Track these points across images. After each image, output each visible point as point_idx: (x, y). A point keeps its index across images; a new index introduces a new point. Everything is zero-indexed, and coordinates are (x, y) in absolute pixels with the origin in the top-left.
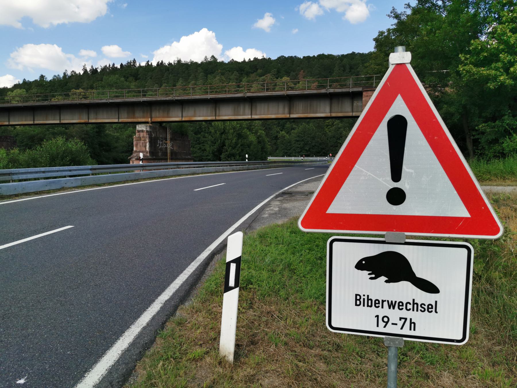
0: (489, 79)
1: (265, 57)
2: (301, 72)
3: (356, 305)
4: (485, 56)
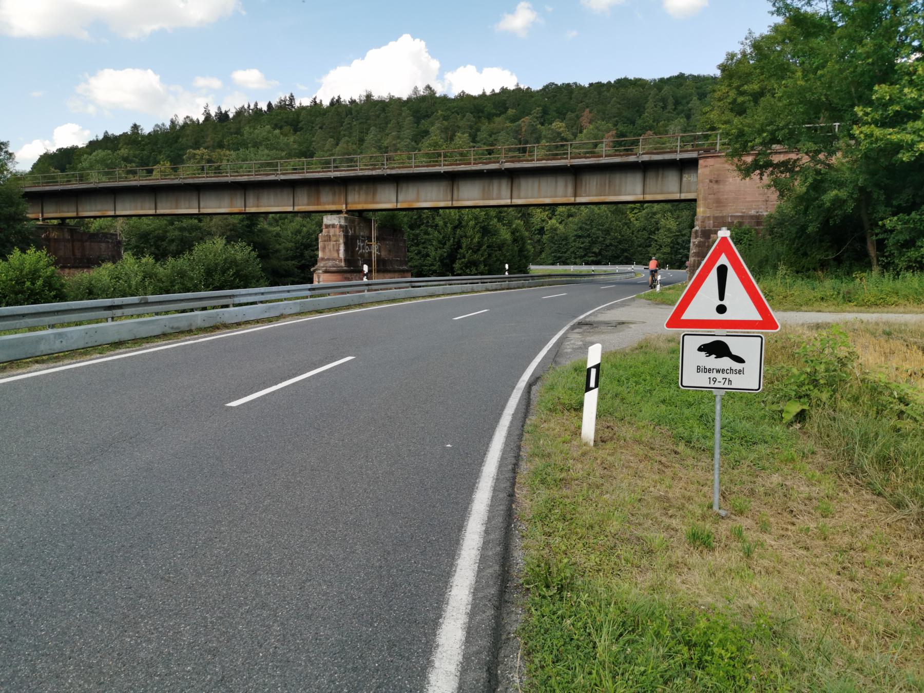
0: (901, 147)
4: (897, 111)
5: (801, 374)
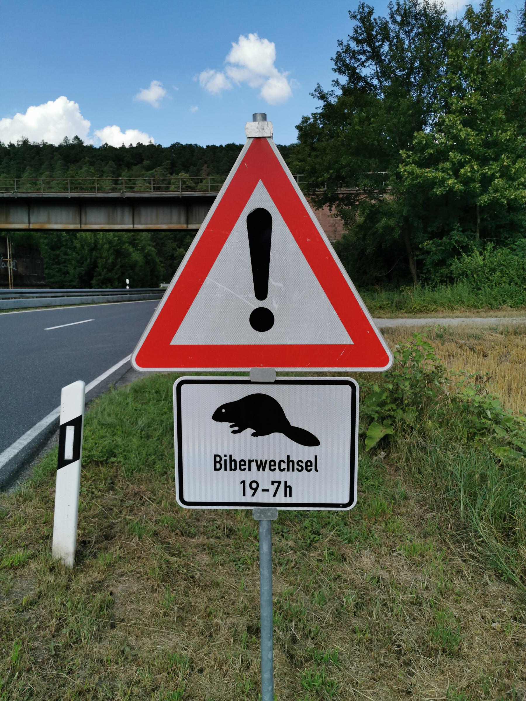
0: (435, 183)
1: (153, 142)
2: (204, 167)
3: (216, 469)
5: (383, 392)
